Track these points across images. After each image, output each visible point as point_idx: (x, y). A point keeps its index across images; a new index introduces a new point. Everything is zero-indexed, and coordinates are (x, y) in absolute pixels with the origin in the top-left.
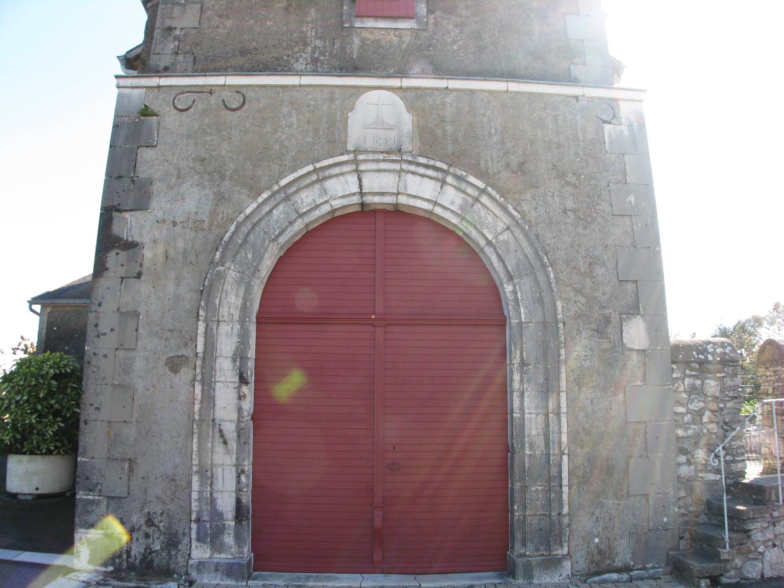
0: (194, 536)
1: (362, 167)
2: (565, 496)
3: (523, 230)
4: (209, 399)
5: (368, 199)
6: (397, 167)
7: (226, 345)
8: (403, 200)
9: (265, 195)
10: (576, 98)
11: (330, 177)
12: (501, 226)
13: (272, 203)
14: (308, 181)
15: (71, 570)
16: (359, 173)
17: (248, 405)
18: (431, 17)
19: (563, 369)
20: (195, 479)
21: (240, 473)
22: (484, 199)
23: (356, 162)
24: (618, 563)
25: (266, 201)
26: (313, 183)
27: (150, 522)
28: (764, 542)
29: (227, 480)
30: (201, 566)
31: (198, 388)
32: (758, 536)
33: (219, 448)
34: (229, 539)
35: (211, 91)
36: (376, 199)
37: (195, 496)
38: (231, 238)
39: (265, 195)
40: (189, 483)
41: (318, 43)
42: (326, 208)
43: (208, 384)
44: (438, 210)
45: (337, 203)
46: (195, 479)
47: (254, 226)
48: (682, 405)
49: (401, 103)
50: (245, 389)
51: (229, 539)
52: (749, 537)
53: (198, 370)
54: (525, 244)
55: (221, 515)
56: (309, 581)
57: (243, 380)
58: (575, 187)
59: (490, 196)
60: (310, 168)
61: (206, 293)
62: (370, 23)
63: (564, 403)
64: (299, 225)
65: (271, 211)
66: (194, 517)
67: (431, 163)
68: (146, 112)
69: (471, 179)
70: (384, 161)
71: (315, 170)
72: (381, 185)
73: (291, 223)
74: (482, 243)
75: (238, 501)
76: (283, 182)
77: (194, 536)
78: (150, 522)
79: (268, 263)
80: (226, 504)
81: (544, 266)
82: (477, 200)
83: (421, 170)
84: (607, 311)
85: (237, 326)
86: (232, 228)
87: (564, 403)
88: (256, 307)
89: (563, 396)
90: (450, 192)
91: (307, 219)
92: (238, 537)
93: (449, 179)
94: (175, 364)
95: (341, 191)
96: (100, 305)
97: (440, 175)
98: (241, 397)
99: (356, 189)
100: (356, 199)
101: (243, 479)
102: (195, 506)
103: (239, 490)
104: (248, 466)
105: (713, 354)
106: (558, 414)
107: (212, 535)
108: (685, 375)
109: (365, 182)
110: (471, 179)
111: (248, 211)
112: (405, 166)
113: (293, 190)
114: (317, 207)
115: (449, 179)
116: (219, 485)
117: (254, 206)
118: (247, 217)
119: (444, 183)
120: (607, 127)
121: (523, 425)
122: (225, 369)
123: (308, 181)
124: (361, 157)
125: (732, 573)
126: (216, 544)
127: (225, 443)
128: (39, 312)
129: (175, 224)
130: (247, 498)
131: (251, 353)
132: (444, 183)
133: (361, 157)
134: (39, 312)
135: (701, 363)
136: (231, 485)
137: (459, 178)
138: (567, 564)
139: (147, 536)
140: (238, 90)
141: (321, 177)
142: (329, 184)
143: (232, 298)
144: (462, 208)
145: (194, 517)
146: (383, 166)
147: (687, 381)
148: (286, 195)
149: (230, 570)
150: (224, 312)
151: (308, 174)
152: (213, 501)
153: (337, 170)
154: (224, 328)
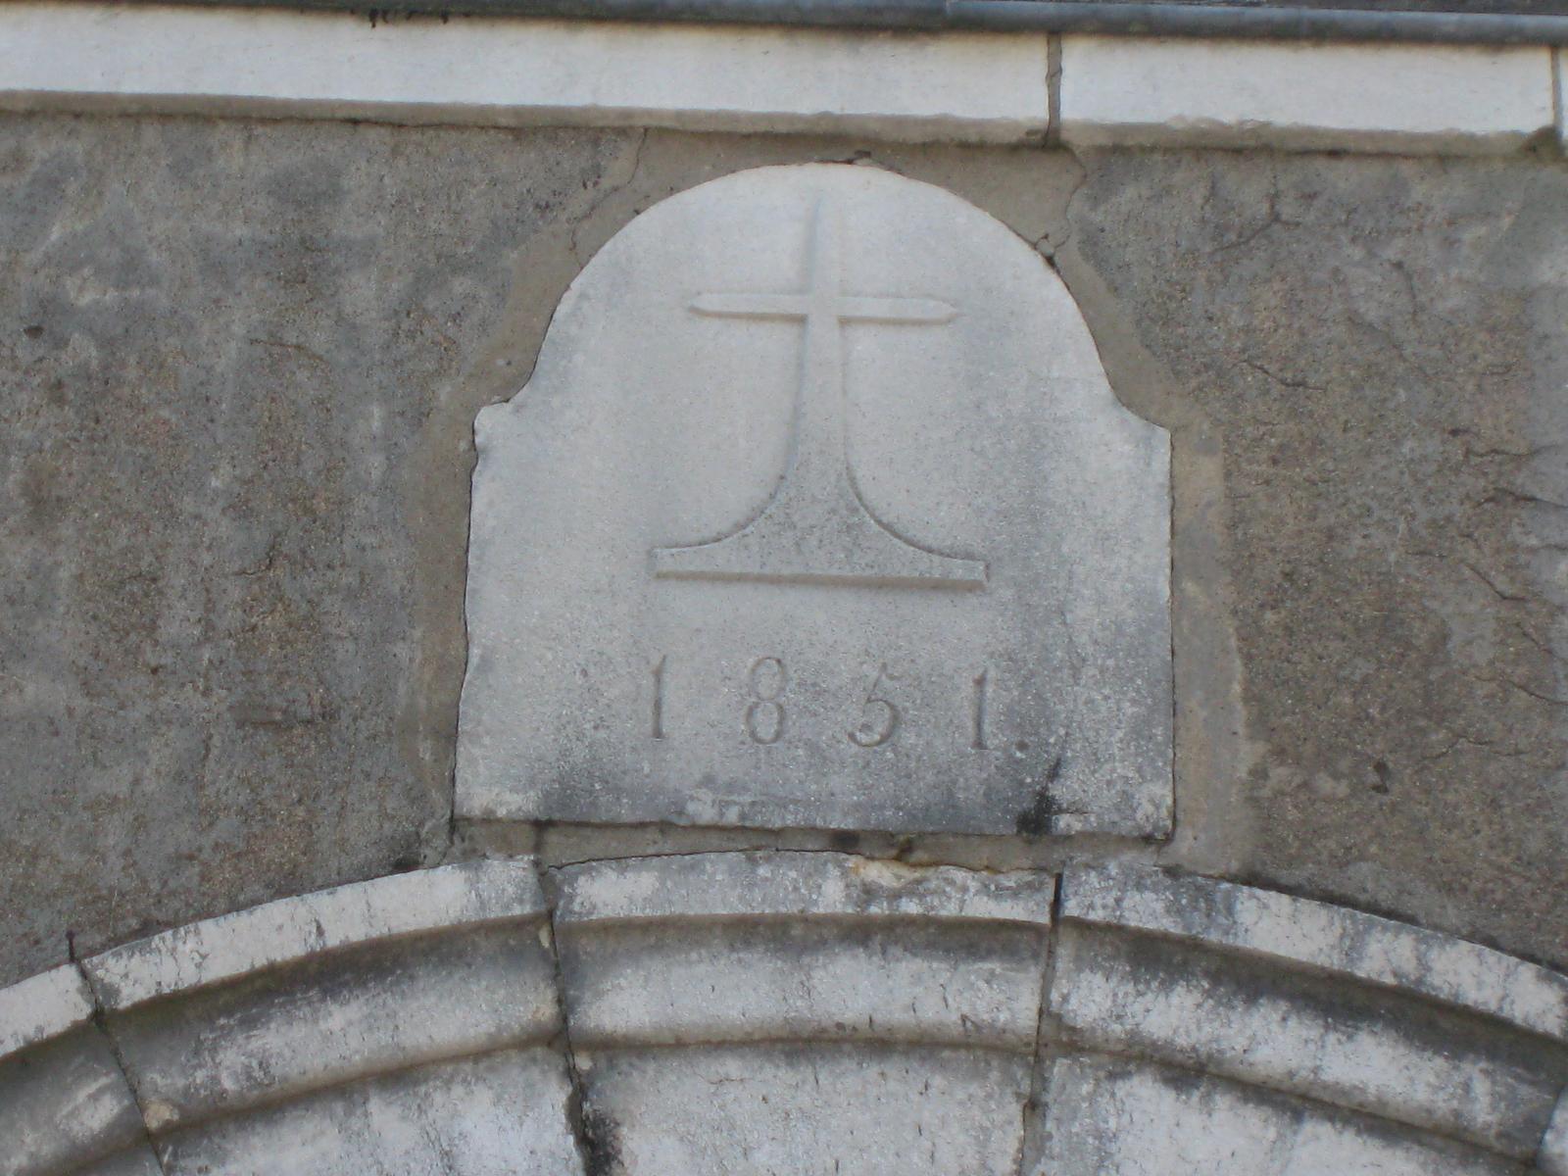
1: (624, 1002)
6: (1004, 999)
67: (1385, 955)
71: (105, 1033)
83: (1276, 1040)
112: (1093, 997)
124: (609, 892)
133: (609, 892)
146: (853, 988)
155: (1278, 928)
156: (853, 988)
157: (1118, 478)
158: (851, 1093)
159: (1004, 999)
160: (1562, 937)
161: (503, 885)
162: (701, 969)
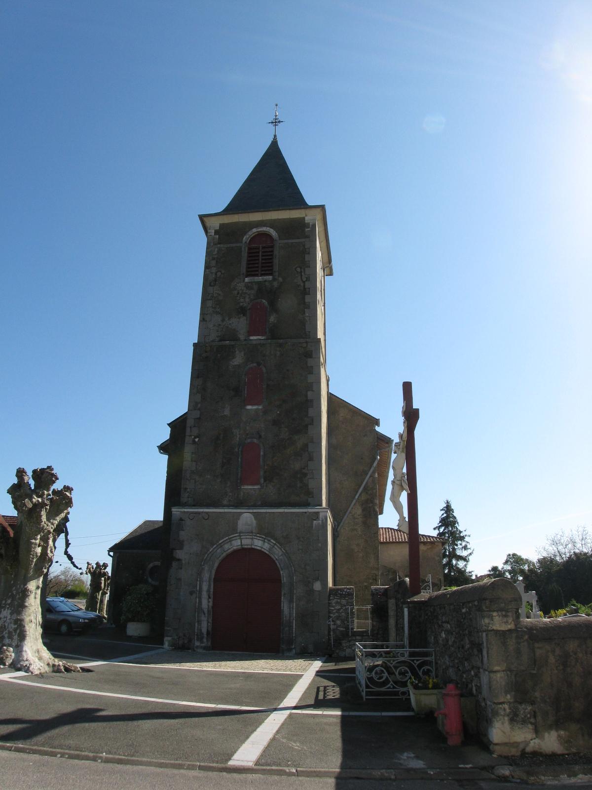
0: (196, 639)
1: (242, 537)
2: (294, 631)
3: (286, 556)
4: (200, 603)
5: (243, 546)
6: (251, 537)
7: (205, 587)
8: (253, 547)
9: (215, 546)
10: (306, 512)
11: (233, 540)
12: (280, 554)
13: (217, 548)
14: (227, 541)
15: (163, 648)
16: (241, 539)
17: (211, 604)
18: (265, 483)
19: (295, 596)
20: (196, 624)
21: (208, 622)
22: (276, 547)
23: (240, 536)
24: (309, 652)
25: (215, 547)
26: (227, 543)
27: (184, 635)
28: (346, 646)
29: (205, 625)
30: (197, 647)
31: (197, 600)
32: (344, 645)
33: (203, 615)
34: (205, 640)
35: (199, 513)
36: (246, 547)
37: (196, 628)
38: (206, 558)
39: (215, 546)
40: (195, 626)
41: (230, 494)
42: (232, 550)
43: (200, 598)
44: (263, 550)
45: (235, 548)
46: (196, 624)
47: (212, 555)
48: (333, 607)
49: (253, 517)
50: (210, 600)
51: (205, 640)
52: (341, 645)
53: (197, 595)
54: (286, 559)
55: (203, 634)
56: (94, 756)
57: (209, 597)
58: (303, 542)
59: (278, 546)
60: (227, 538)
61: (200, 573)
62: (246, 487)
63: (294, 605)
64: (224, 554)
65: (216, 551)
66: (196, 634)
67: (261, 536)
68: (181, 519)
69: (272, 541)
70: (248, 535)
71: (229, 539)
72: (247, 542)
73: (222, 554)
74: (275, 559)
75: (208, 630)
76: (220, 542)
77: (196, 639)
78: (184, 635)
79: (216, 565)
80: (204, 631)
81: (291, 566)
82: (273, 547)
83: (258, 538)
84: (309, 579)
85: (208, 583)
86: (206, 555)
87: (294, 605)
88: (213, 577)
89: (295, 604)
90: (266, 544)
91: (227, 552)
92: (207, 641)
93: (266, 541)
94: (191, 593)
95: (236, 544)
96: (171, 576)
97: (263, 539)
98: (209, 602)
99: (240, 544)
100: (240, 547)
101: (209, 624)
102: (196, 631)
103: (208, 627)
104: (210, 620)
105: (346, 592)
106: (293, 608)
107: (200, 639)
108: (335, 598)
109: (243, 542)
110: (272, 541)
111: (210, 551)
112: (253, 537)
113: (222, 544)
114: (229, 549)
115: (266, 541)
116: (203, 625)
117: (212, 549)
118: (210, 552)
119: (264, 542)
120: (315, 522)
121: (283, 611)
122: (205, 594)
123: (227, 541)
124: (241, 534)
125: (335, 654)
126: (202, 642)
127: (204, 614)
128: (112, 555)
129: (191, 554)
130: (210, 629)
131: (212, 590)
132: (264, 542)
133: (241, 534)
134: (112, 555)
135: (341, 595)
136: (206, 626)
137: (269, 541)
138: (294, 651)
139: (183, 639)
140: (207, 513)
141: (230, 540)
142: (233, 542)
143: (206, 575)
144: (269, 549)
145: (196, 634)
146: (247, 537)
147: (335, 600)
148: (221, 546)
149: (205, 648)
150: (204, 579)
151: (227, 540)
152: (201, 630)
153: (235, 538)
154: (204, 583)
155: (258, 535)
156: (247, 537)
157: (254, 522)
158: (248, 539)
159: (251, 537)
160: (14, 574)
161: (238, 534)
162: (26, 643)
